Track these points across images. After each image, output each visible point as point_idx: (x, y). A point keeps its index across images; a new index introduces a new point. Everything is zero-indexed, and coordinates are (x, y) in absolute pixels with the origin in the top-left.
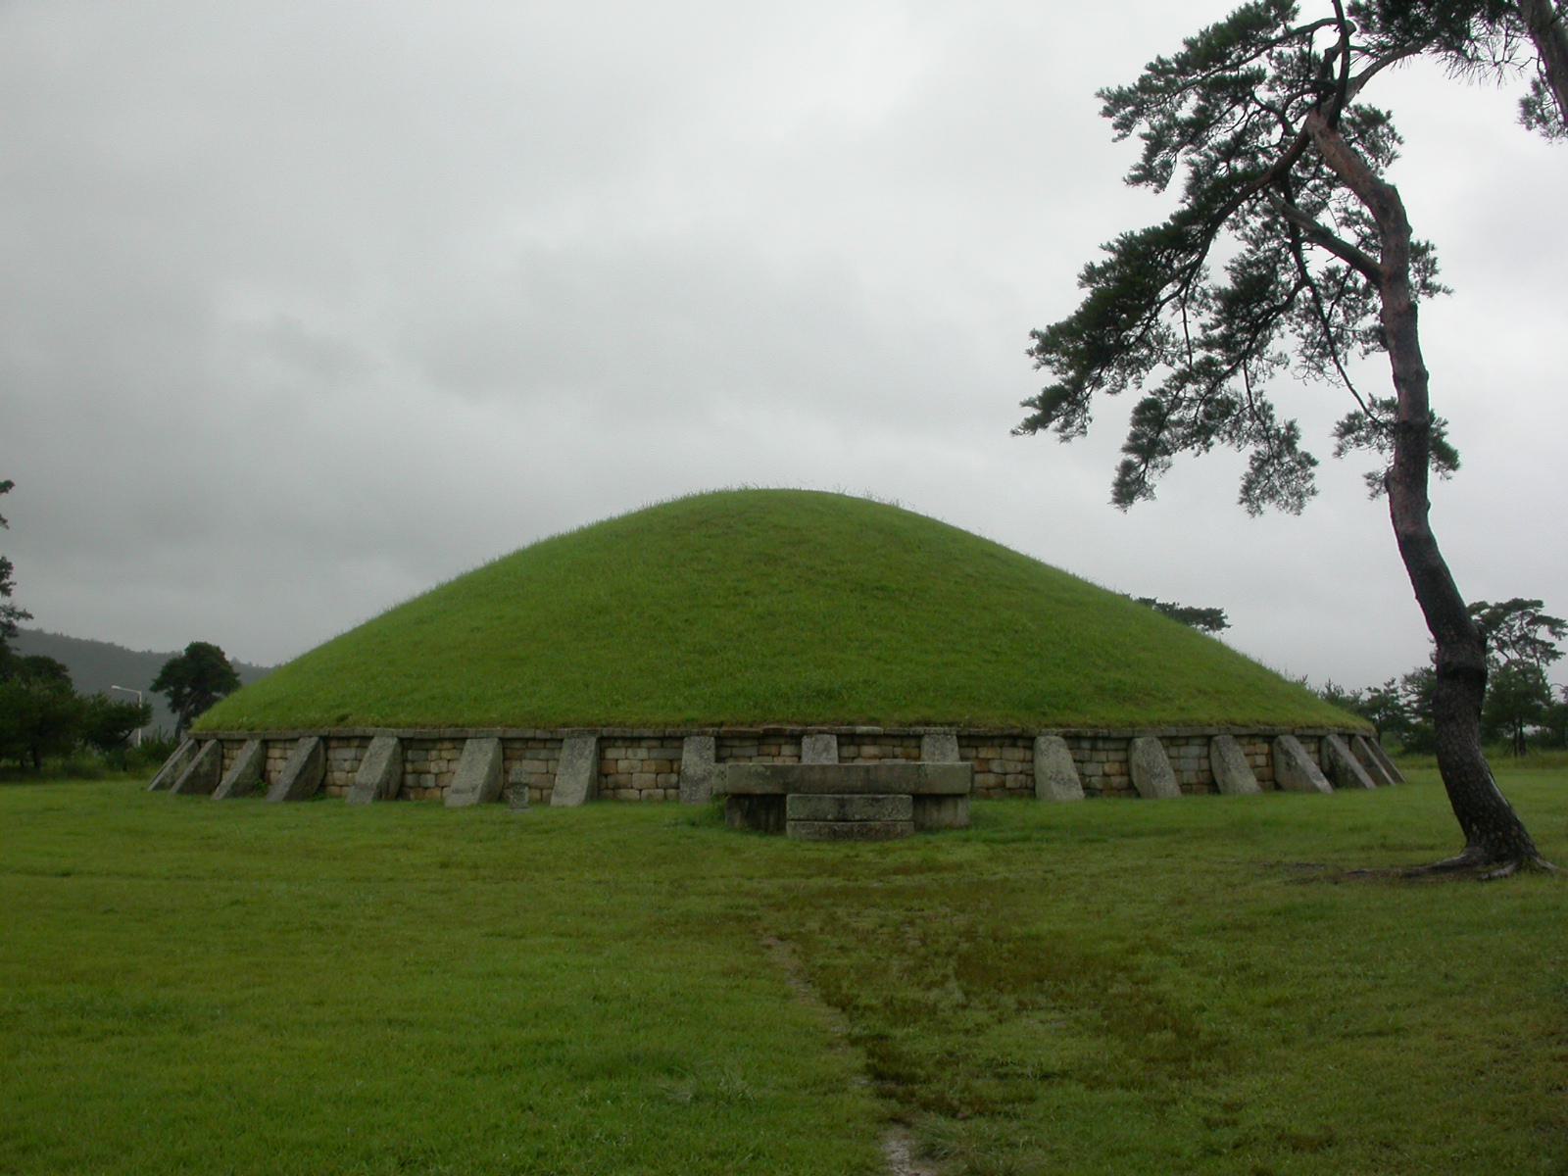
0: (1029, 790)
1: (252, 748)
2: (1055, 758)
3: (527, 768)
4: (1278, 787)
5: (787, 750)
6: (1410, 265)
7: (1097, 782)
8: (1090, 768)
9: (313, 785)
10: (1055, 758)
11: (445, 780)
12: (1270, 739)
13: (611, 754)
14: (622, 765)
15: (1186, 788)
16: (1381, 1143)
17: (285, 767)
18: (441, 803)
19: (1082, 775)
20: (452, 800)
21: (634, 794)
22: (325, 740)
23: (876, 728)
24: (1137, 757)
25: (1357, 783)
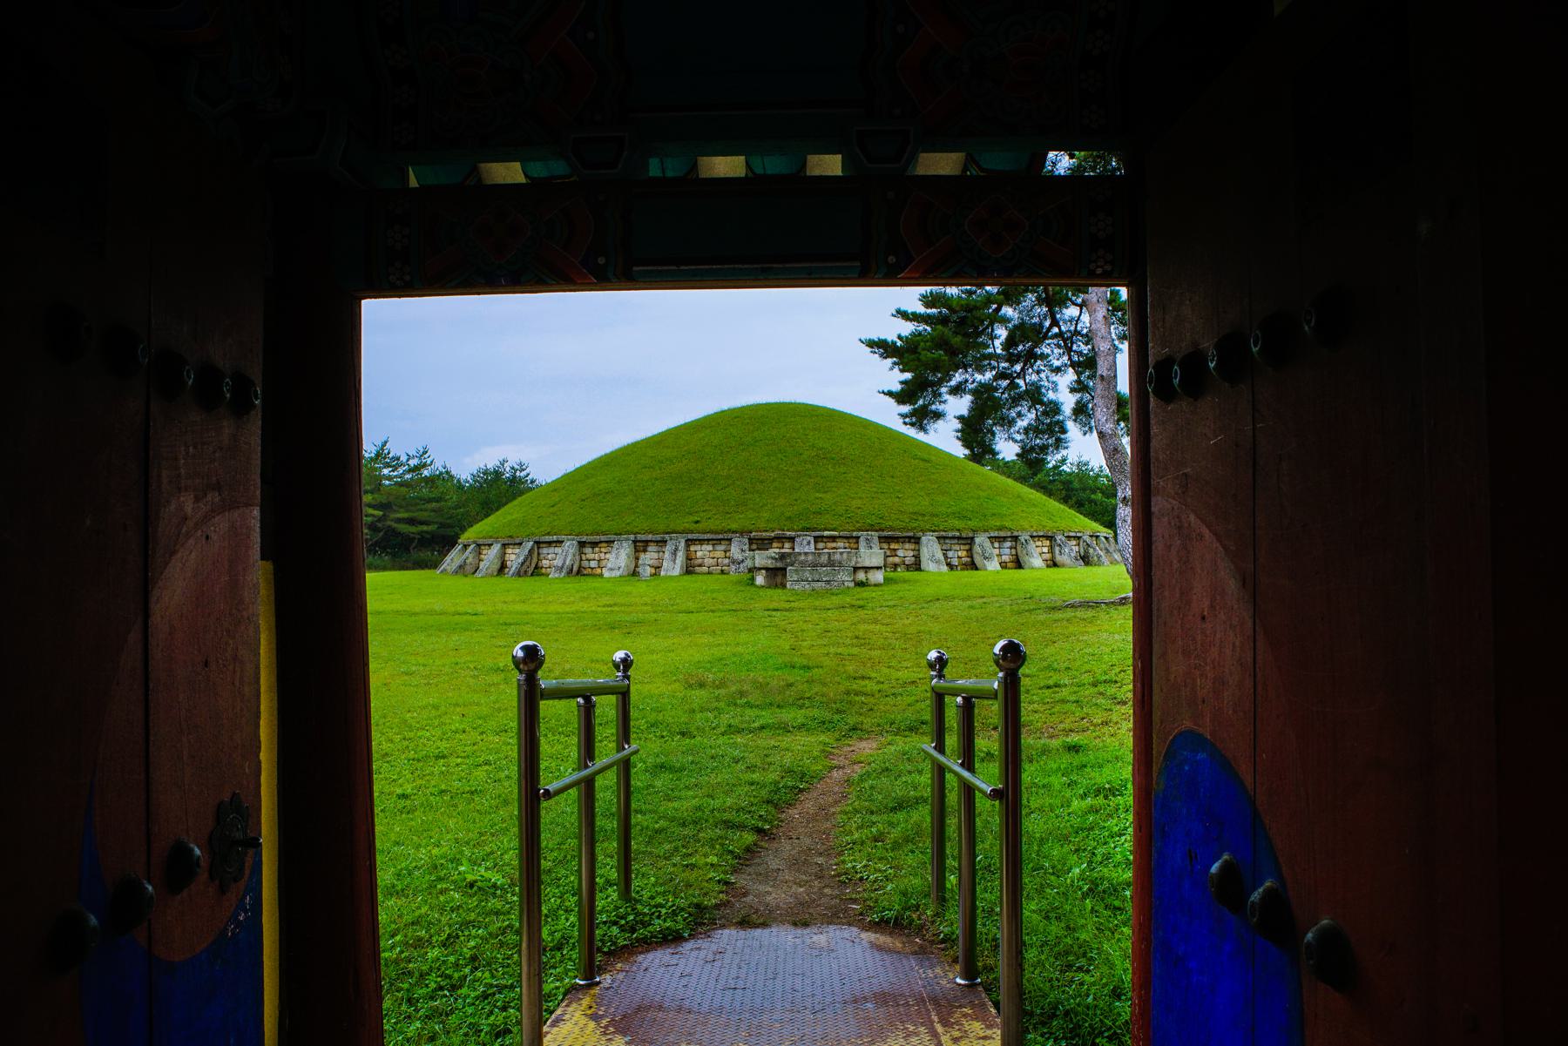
0: (917, 566)
1: (496, 548)
2: (931, 548)
3: (649, 557)
4: (1055, 565)
5: (787, 545)
6: (1031, 297)
7: (955, 562)
8: (950, 554)
9: (532, 569)
10: (931, 548)
11: (603, 563)
12: (1051, 538)
13: (692, 548)
14: (699, 554)
15: (1004, 565)
16: (510, 1032)
17: (515, 557)
18: (601, 575)
19: (946, 557)
20: (606, 574)
21: (705, 569)
22: (538, 543)
23: (263, 642)
24: (977, 549)
25: (1099, 563)
